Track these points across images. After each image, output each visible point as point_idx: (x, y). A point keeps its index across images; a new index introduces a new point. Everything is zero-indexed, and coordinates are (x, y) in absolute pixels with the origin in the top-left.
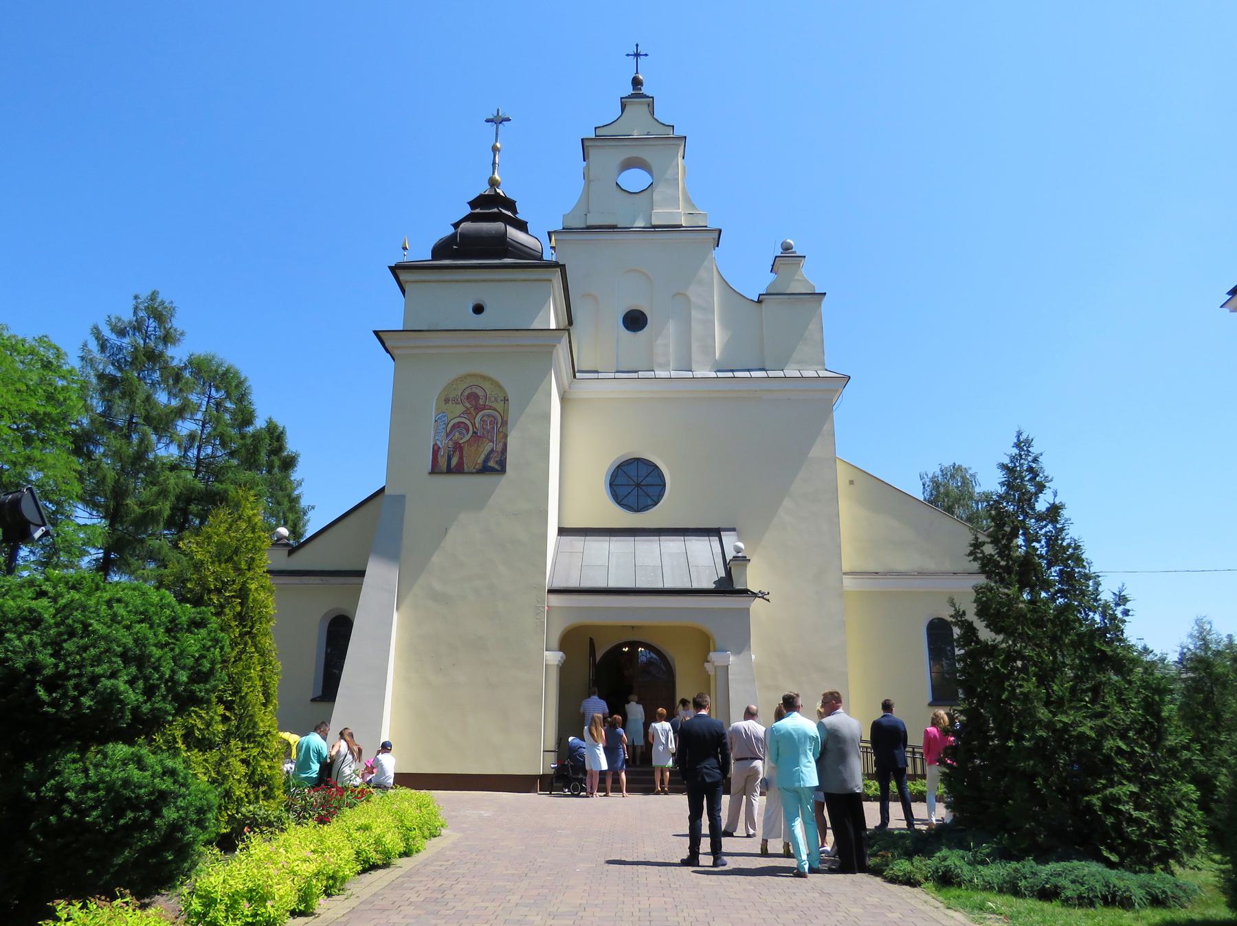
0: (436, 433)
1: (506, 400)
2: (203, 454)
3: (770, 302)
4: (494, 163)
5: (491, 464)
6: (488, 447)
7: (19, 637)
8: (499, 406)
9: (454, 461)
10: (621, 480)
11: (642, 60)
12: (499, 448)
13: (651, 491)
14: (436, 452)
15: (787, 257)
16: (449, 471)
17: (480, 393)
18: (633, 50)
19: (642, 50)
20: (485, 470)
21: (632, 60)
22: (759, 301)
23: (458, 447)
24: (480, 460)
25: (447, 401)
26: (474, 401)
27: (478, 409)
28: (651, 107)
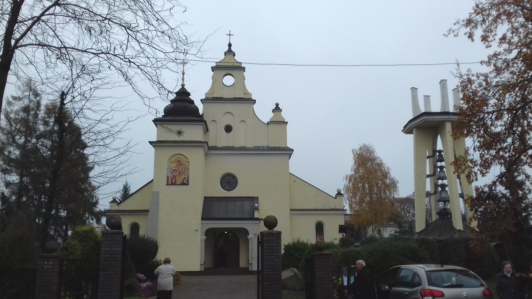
0: (168, 172)
1: (189, 162)
2: (116, 29)
3: (270, 125)
4: (183, 74)
5: (185, 182)
6: (184, 176)
7: (478, 170)
8: (187, 164)
9: (173, 181)
10: (231, 178)
11: (231, 36)
12: (187, 177)
13: (227, 187)
14: (168, 178)
15: (277, 109)
16: (172, 184)
17: (181, 160)
18: (228, 33)
19: (231, 33)
20: (183, 184)
21: (228, 36)
22: (268, 124)
23: (174, 177)
24: (181, 180)
25: (171, 162)
26: (179, 163)
27: (180, 165)
28: (234, 55)
